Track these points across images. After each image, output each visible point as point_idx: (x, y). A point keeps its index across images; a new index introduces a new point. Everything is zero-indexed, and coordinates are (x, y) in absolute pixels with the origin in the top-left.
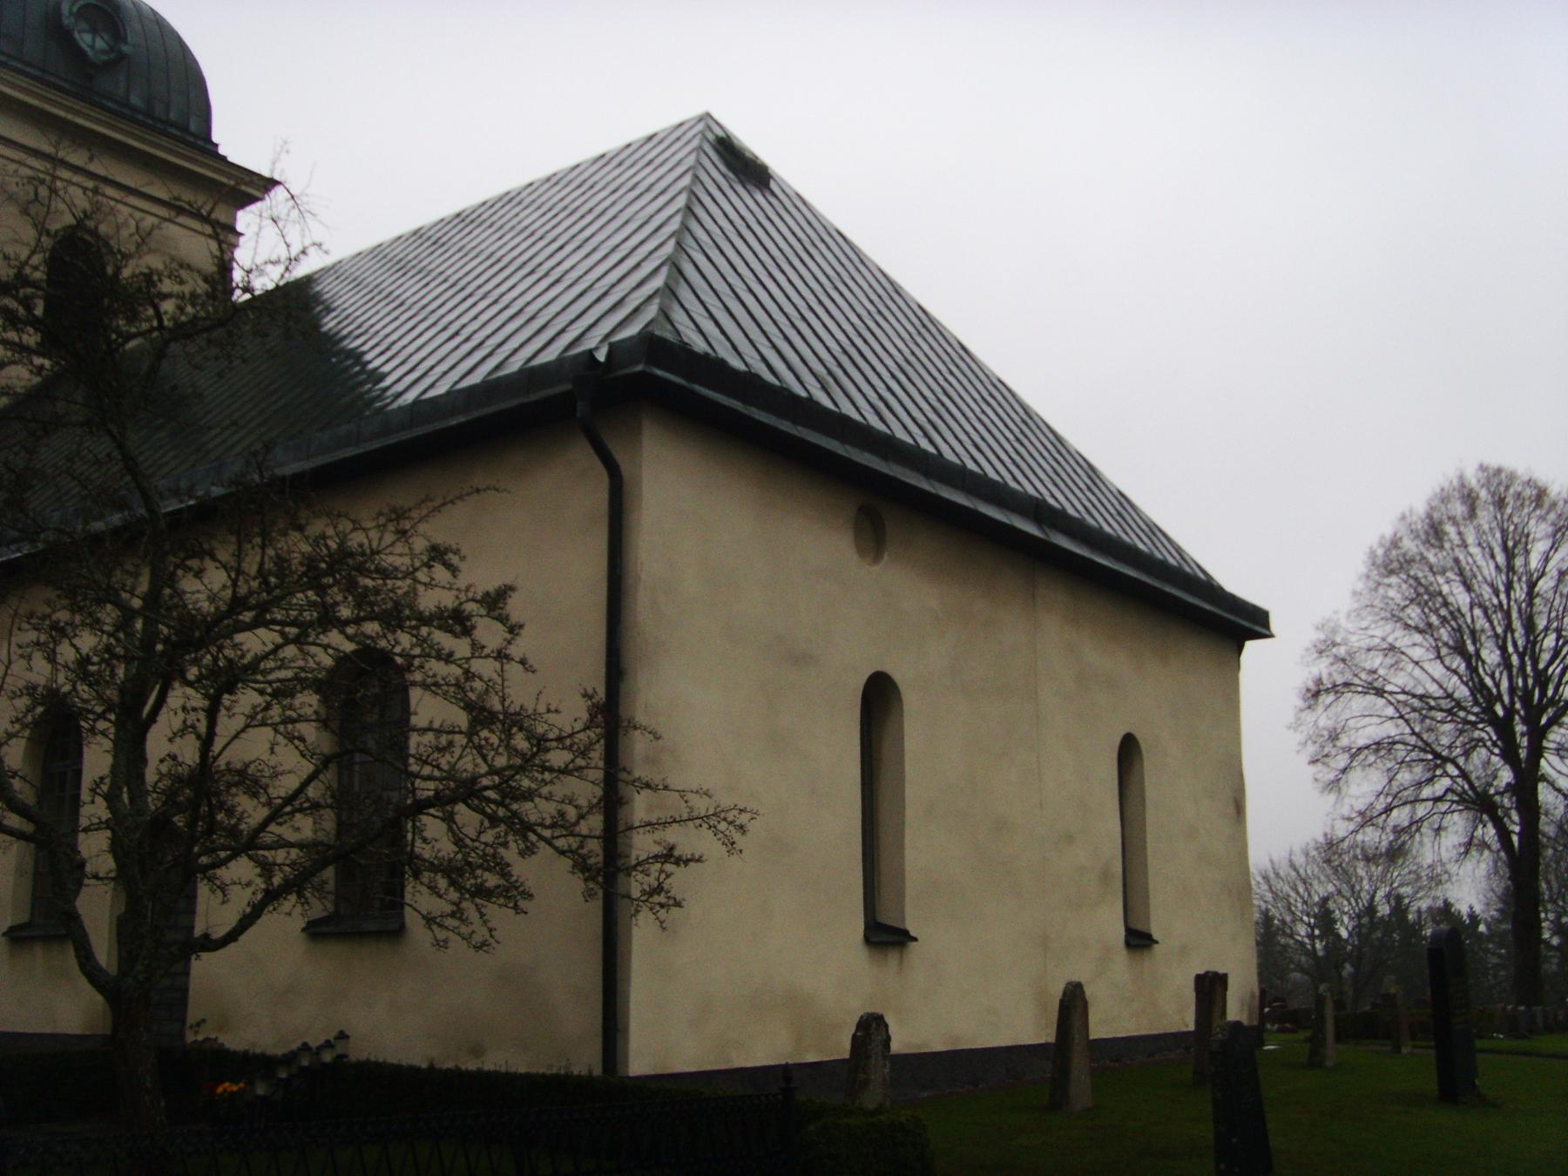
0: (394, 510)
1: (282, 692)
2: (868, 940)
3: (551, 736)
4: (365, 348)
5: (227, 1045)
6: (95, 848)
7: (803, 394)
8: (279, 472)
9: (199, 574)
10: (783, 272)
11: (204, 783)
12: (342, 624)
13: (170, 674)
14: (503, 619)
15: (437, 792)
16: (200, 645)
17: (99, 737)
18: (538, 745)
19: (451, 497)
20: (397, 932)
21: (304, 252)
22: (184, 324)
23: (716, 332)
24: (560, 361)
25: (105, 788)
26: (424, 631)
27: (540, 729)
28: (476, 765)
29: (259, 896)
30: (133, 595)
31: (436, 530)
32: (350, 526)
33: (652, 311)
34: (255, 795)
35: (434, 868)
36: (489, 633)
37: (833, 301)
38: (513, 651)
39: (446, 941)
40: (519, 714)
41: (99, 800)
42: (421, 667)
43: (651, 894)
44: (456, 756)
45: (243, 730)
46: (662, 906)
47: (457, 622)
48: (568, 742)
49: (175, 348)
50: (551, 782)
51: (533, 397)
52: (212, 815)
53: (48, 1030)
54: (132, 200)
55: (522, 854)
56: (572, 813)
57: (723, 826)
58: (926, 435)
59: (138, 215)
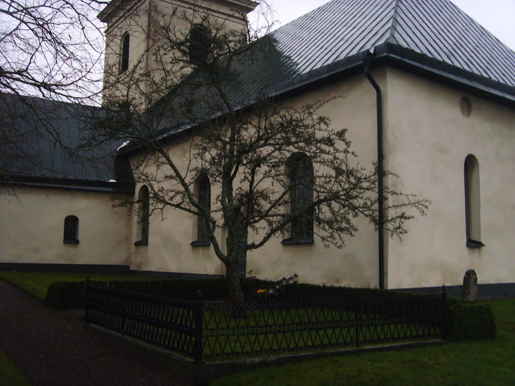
0: (308, 106)
1: (275, 166)
2: (468, 245)
3: (363, 177)
4: (292, 55)
5: (259, 278)
6: (218, 217)
7: (441, 60)
8: (270, 95)
9: (246, 129)
10: (432, 18)
11: (251, 197)
12: (292, 144)
13: (239, 162)
14: (344, 140)
15: (325, 198)
16: (247, 152)
17: (218, 183)
18: (358, 181)
19: (326, 100)
20: (310, 243)
21: (273, 23)
22: (237, 50)
23: (410, 40)
24: (358, 54)
25: (220, 198)
26: (319, 145)
27: (359, 176)
28: (338, 188)
29: (269, 231)
30: (225, 137)
31: (321, 112)
32: (294, 112)
33: (388, 35)
34: (266, 200)
35: (325, 222)
36: (340, 145)
37: (450, 27)
38: (349, 150)
39: (328, 245)
40: (352, 170)
41: (218, 202)
42: (320, 156)
43: (397, 229)
44: (332, 184)
45: (263, 179)
46: (401, 233)
47: (329, 141)
48: (368, 179)
49: (235, 58)
50: (363, 193)
51: (350, 67)
52: (253, 206)
53: (205, 273)
54: (215, 14)
55: (354, 216)
56: (369, 203)
57: (420, 206)
58: (485, 72)
59: (216, 18)
